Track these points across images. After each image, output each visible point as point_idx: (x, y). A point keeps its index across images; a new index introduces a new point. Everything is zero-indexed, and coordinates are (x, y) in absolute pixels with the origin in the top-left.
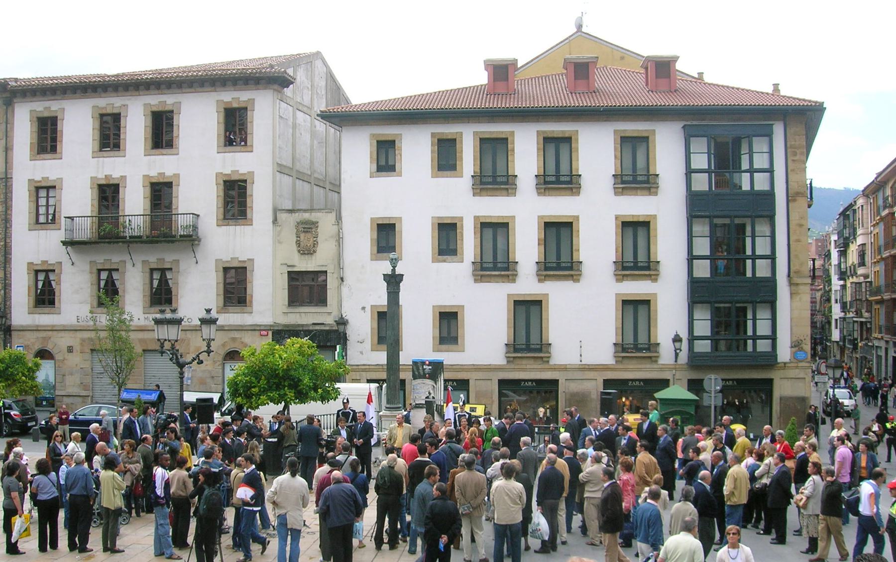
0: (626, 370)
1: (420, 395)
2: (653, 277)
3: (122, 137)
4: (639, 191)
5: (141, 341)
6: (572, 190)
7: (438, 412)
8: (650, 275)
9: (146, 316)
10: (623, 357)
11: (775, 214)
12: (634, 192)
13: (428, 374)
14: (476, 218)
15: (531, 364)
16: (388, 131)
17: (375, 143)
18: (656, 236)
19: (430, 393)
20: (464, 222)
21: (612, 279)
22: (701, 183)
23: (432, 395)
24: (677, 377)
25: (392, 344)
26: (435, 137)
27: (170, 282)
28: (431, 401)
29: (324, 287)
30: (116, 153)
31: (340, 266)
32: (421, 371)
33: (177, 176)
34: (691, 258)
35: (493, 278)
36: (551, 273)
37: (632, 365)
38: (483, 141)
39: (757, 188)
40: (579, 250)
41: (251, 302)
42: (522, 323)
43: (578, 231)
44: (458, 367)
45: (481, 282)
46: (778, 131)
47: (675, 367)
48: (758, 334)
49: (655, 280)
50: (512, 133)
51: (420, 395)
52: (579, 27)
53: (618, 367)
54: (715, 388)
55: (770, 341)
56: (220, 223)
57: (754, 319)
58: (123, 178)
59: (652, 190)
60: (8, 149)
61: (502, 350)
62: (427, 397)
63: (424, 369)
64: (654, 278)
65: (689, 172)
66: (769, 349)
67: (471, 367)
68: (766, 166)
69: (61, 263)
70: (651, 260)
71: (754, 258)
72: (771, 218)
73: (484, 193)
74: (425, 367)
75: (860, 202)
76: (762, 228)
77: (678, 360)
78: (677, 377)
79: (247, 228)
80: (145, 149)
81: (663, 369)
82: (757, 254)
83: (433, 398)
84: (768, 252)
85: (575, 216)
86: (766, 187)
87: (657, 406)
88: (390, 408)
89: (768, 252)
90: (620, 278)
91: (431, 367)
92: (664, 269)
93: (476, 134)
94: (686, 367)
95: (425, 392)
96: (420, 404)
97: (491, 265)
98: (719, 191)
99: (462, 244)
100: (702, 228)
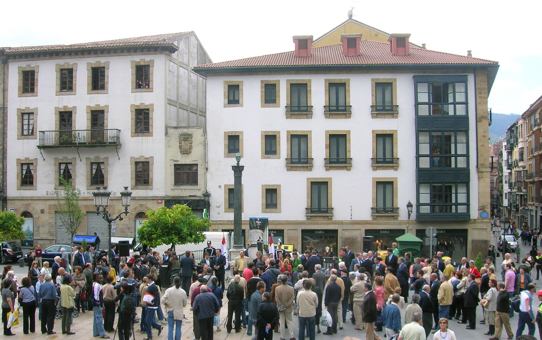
0: (379, 224)
1: (254, 239)
2: (395, 168)
3: (74, 83)
4: (386, 116)
5: (86, 206)
6: (346, 115)
7: (265, 249)
8: (393, 167)
9: (88, 191)
10: (377, 216)
11: (469, 130)
12: (384, 116)
13: (259, 226)
14: (288, 132)
15: (321, 220)
16: (234, 79)
17: (227, 87)
18: (397, 143)
19: (260, 238)
20: (281, 135)
21: (370, 169)
22: (424, 111)
23: (261, 239)
24: (410, 228)
25: (237, 208)
26: (263, 83)
27: (103, 171)
28: (261, 243)
29: (196, 174)
30: (70, 93)
31: (205, 161)
32: (255, 225)
33: (107, 106)
34: (418, 156)
35: (298, 168)
36: (334, 165)
37: (382, 221)
38: (292, 85)
39: (458, 113)
40: (350, 151)
41: (152, 183)
42: (316, 196)
43: (350, 140)
44: (277, 222)
45: (291, 171)
46: (471, 79)
47: (408, 222)
48: (458, 202)
49: (396, 170)
50: (310, 81)
51: (254, 239)
52: (351, 16)
53: (374, 222)
54: (433, 235)
55: (466, 206)
56: (133, 135)
57: (456, 193)
58: (75, 108)
59: (395, 115)
60: (5, 90)
61: (304, 212)
62: (258, 240)
63: (256, 224)
64: (396, 168)
65: (417, 104)
66: (465, 211)
67: (285, 222)
68: (463, 100)
69: (37, 159)
70: (394, 157)
71: (456, 156)
72: (466, 132)
73: (293, 117)
74: (257, 222)
75: (520, 122)
76: (461, 138)
77: (410, 218)
78: (410, 228)
79: (150, 138)
80: (88, 90)
81: (401, 223)
82: (458, 154)
83: (262, 241)
84: (465, 153)
85: (348, 131)
86: (463, 113)
87: (397, 246)
88: (236, 247)
89: (465, 153)
90: (375, 168)
91: (260, 222)
92: (401, 163)
93: (288, 81)
94: (415, 222)
95: (257, 237)
96: (254, 244)
97: (297, 161)
98: (435, 115)
99: (280, 148)
100: (425, 138)
